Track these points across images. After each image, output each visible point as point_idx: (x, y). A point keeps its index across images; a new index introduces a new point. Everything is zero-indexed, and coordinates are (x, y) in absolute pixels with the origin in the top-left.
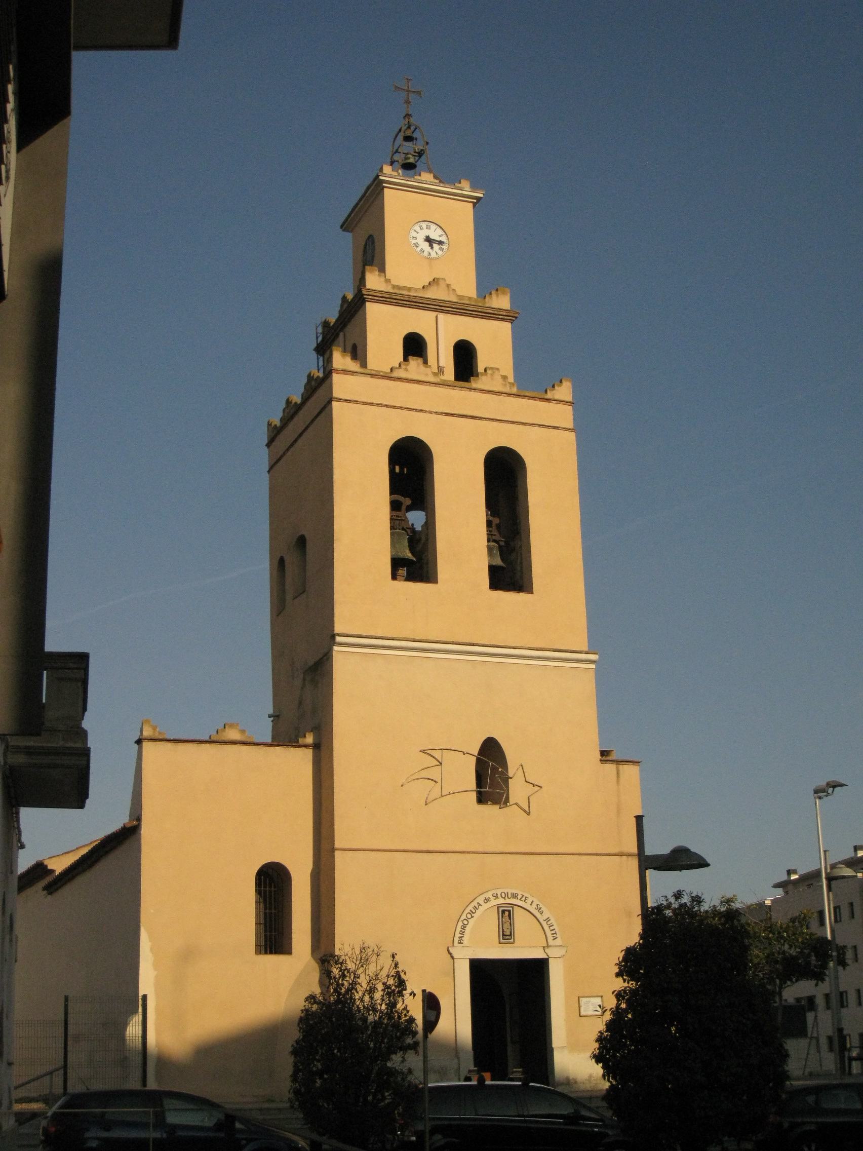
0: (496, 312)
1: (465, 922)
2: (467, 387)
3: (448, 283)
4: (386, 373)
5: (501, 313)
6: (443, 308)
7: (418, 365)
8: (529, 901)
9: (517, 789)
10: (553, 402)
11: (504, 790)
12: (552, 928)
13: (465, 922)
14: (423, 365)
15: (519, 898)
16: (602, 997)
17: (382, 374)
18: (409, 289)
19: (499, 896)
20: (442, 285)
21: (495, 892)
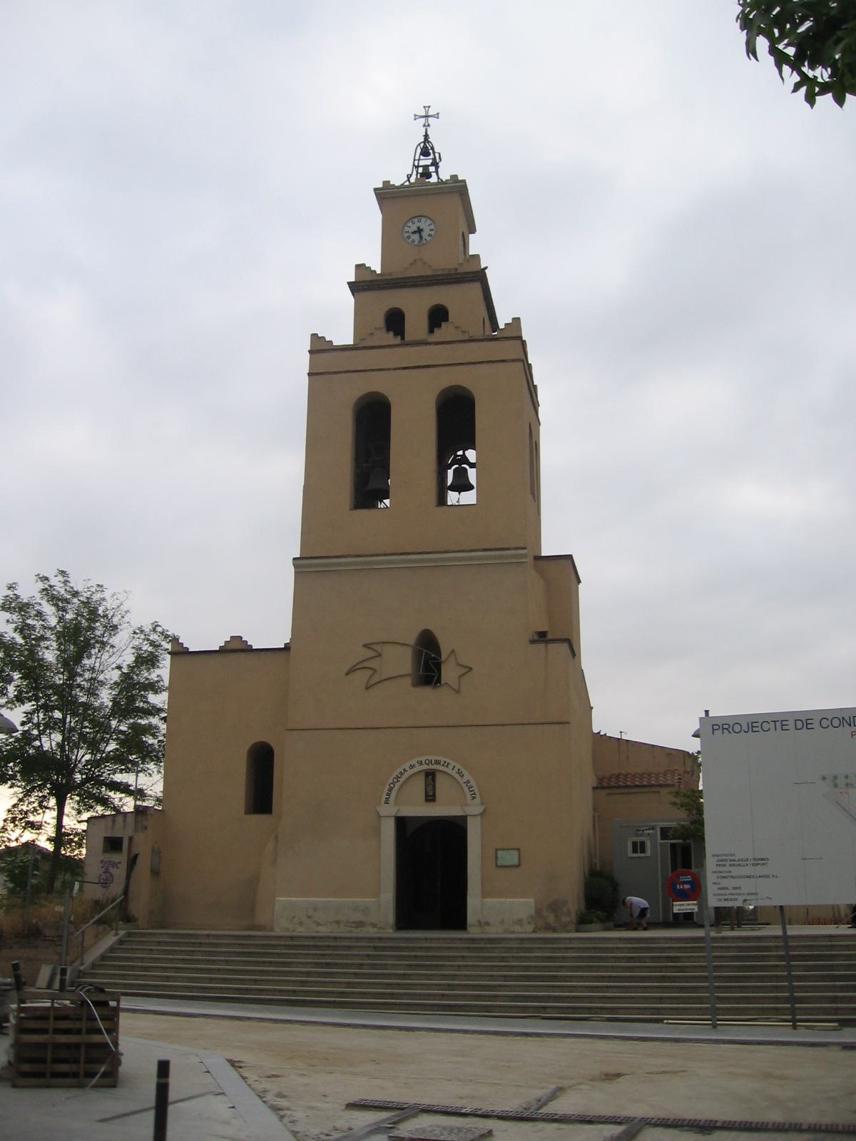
1: (392, 786)
8: (451, 767)
9: (449, 673)
11: (434, 672)
12: (471, 789)
13: (392, 786)
15: (442, 764)
16: (518, 849)
19: (423, 763)
21: (419, 759)
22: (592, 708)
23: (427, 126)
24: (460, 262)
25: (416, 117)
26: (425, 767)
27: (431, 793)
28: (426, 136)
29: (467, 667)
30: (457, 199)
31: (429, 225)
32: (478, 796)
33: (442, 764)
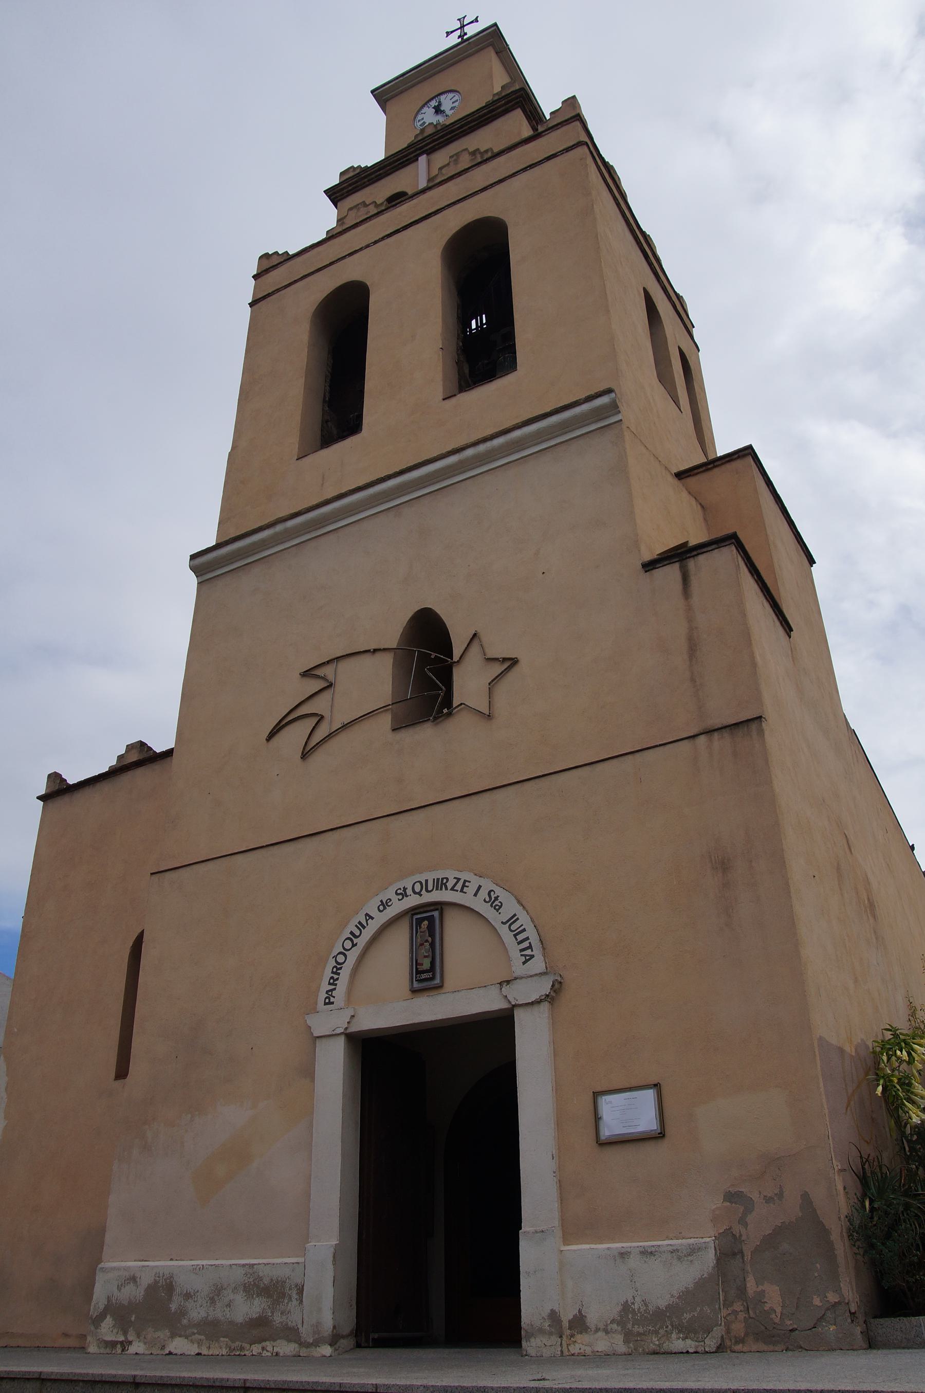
1: (341, 959)
8: (471, 889)
12: (520, 937)
13: (341, 959)
15: (450, 885)
19: (409, 892)
22: (912, 848)
26: (412, 901)
27: (426, 964)
29: (505, 660)
30: (490, 57)
32: (537, 952)
33: (450, 885)
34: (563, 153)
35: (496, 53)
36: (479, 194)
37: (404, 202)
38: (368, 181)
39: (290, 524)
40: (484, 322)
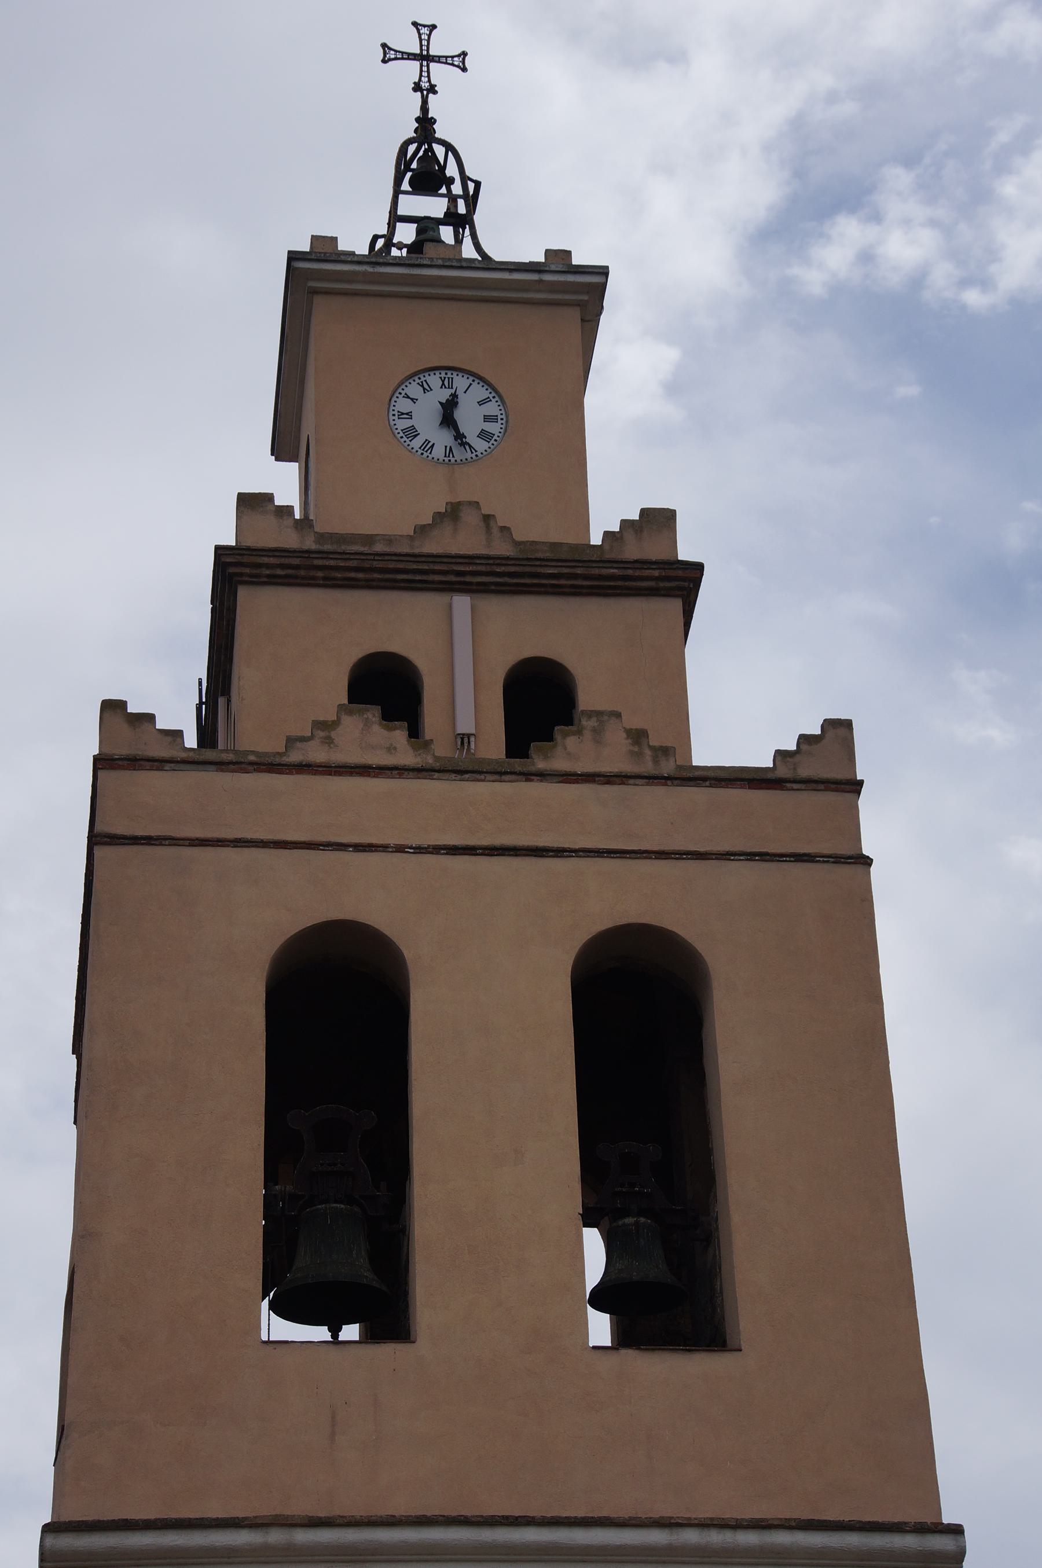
0: (630, 572)
2: (518, 769)
3: (485, 511)
4: (497, 761)
5: (647, 573)
6: (468, 579)
7: (367, 723)
10: (795, 786)
14: (380, 724)
17: (252, 758)
18: (369, 539)
20: (470, 518)
23: (425, 90)
24: (461, 729)
25: (388, 54)
28: (425, 124)
31: (481, 403)
34: (828, 862)
35: (581, 319)
36: (651, 858)
37: (482, 777)
38: (325, 578)
39: (302, 1536)
40: (204, 700)
